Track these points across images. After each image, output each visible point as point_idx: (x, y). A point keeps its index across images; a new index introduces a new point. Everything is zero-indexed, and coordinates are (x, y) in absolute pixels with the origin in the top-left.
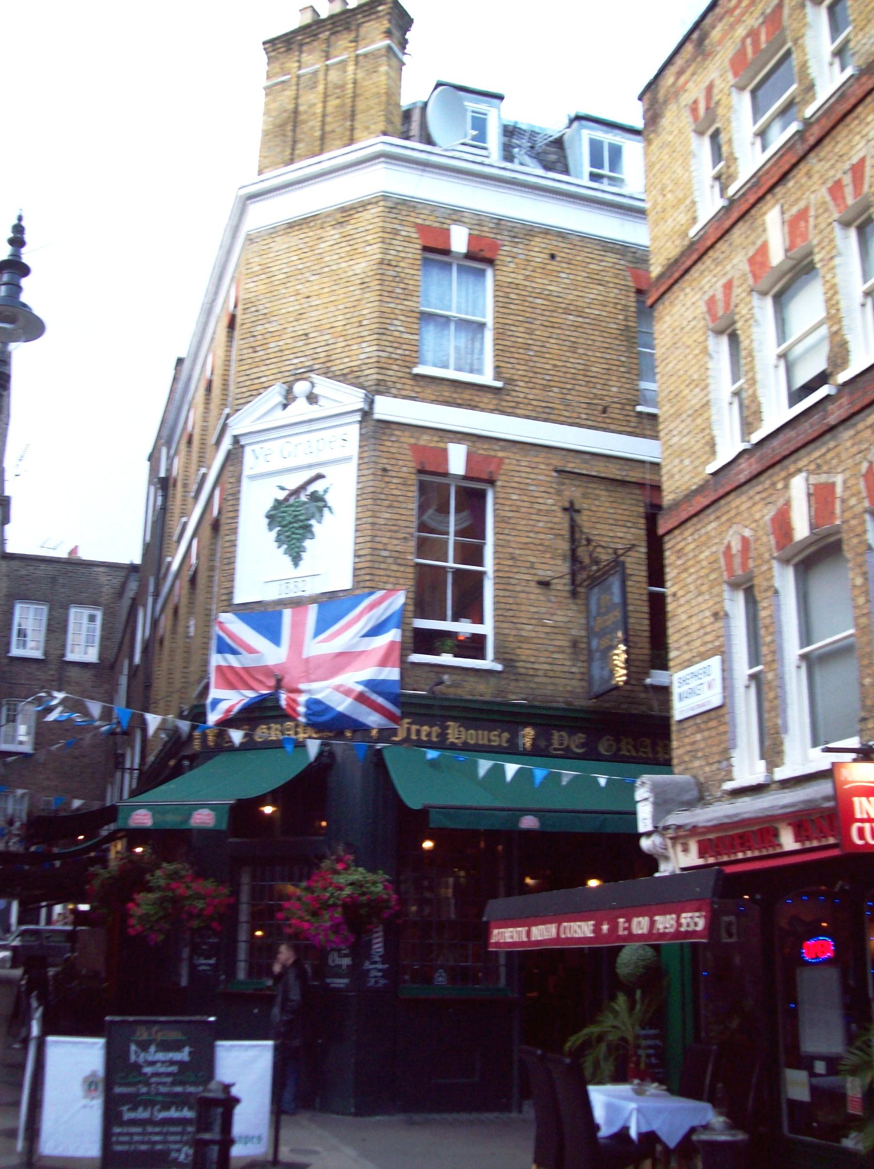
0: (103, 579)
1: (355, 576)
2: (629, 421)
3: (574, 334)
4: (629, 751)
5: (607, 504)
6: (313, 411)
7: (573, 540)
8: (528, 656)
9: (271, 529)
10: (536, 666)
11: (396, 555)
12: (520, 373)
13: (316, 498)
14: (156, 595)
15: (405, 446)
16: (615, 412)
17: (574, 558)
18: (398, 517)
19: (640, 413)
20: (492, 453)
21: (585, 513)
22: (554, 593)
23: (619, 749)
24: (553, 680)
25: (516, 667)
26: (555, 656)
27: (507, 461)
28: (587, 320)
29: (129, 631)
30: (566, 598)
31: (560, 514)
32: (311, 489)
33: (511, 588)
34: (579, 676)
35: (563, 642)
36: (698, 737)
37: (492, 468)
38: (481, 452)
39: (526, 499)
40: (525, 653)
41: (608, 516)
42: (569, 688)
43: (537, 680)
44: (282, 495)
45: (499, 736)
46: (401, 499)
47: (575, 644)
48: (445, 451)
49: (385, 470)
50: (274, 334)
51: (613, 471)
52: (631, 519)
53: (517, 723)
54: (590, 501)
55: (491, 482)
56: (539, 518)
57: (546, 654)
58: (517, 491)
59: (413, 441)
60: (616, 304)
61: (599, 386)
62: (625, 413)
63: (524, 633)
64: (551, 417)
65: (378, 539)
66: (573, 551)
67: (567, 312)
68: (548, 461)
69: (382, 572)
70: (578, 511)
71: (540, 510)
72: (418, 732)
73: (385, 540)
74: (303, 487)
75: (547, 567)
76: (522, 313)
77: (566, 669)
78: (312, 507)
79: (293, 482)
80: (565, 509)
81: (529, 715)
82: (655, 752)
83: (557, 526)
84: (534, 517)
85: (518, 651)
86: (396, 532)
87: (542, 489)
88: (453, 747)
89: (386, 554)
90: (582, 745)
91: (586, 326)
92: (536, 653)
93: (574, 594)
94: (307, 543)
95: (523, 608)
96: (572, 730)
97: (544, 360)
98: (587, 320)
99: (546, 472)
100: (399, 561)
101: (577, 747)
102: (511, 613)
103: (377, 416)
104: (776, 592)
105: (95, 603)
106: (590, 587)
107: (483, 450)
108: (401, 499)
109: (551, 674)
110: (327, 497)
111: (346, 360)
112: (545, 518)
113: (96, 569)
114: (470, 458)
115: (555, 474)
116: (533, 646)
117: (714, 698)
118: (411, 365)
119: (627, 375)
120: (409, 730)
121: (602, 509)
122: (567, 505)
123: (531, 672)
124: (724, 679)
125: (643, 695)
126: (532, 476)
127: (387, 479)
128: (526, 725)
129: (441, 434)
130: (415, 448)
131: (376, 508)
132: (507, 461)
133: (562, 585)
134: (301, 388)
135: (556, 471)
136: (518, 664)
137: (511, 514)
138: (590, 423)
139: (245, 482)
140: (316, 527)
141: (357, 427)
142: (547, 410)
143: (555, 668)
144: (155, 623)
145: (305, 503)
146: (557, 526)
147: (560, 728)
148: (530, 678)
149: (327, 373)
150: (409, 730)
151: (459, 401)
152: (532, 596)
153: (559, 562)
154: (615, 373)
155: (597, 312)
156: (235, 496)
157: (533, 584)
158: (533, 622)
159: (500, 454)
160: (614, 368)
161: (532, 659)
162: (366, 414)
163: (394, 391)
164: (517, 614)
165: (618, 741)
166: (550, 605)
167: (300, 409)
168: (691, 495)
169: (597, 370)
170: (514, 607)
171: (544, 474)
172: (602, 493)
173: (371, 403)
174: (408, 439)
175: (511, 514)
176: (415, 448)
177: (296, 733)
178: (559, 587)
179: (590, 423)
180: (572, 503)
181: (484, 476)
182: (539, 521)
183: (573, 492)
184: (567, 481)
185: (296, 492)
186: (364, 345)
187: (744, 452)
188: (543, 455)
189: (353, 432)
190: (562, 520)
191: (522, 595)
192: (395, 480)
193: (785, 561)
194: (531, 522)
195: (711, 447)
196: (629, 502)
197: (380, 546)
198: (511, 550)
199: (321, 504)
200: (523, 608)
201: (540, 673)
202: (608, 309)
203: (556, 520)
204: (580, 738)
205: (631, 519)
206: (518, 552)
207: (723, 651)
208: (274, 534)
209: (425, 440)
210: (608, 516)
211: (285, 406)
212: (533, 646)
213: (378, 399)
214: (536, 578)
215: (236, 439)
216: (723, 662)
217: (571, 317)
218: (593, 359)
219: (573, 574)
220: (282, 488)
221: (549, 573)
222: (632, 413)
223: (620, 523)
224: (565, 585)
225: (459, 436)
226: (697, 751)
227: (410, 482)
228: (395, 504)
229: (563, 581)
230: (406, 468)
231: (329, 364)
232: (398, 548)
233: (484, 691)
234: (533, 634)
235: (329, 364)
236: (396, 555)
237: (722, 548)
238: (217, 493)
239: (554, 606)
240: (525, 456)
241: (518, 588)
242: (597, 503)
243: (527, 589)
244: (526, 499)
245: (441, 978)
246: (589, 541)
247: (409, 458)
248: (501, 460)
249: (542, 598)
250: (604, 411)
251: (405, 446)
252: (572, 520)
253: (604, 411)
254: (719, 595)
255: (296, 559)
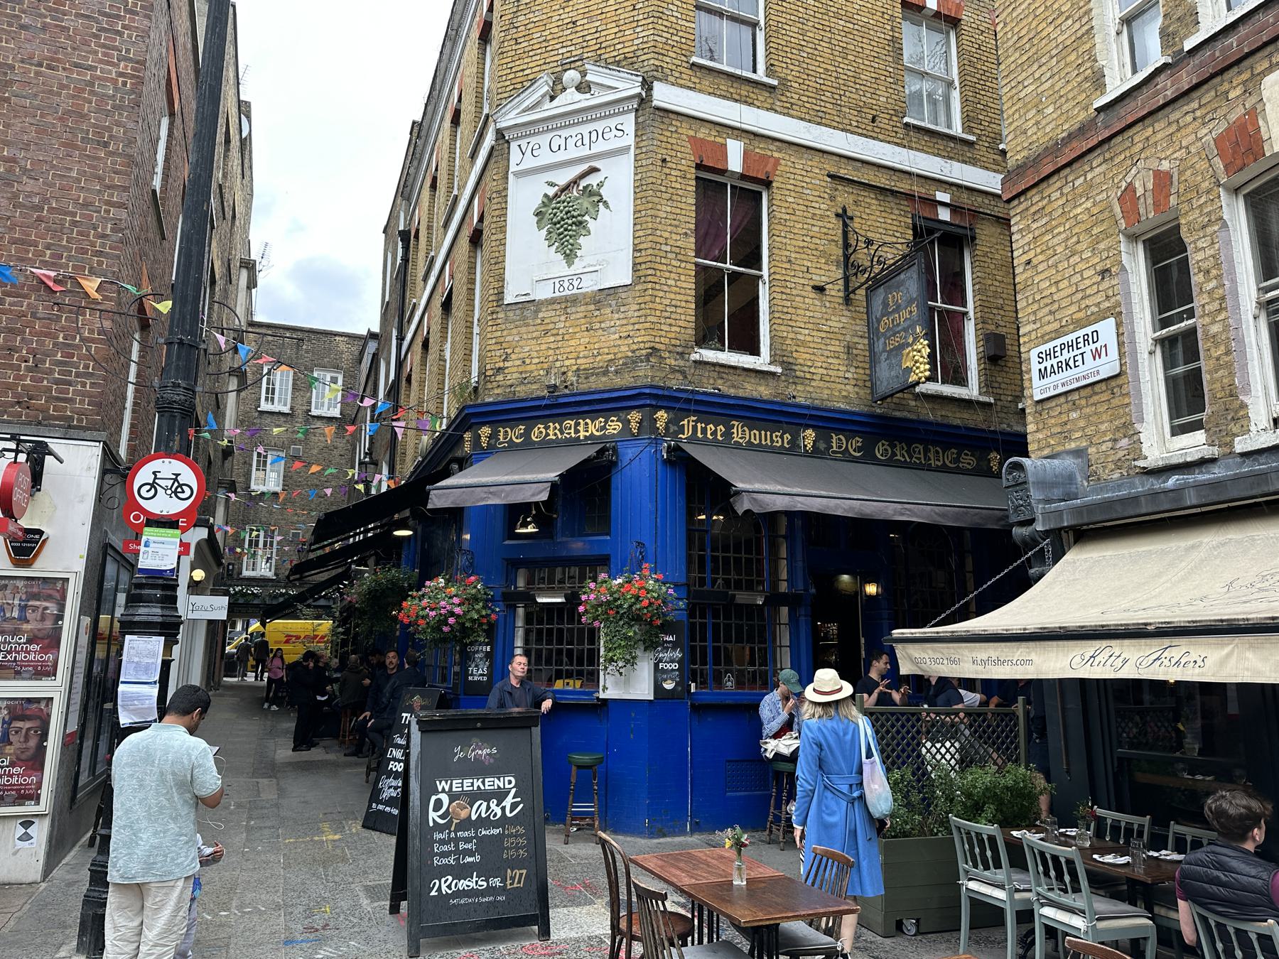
0: (343, 347)
1: (634, 271)
2: (896, 132)
3: (844, 39)
4: (904, 457)
5: (878, 213)
6: (584, 100)
7: (846, 245)
8: (805, 360)
9: (540, 228)
10: (812, 370)
11: (677, 250)
12: (793, 73)
13: (588, 192)
14: (401, 339)
15: (684, 137)
16: (883, 121)
17: (847, 261)
18: (678, 211)
19: (907, 125)
20: (769, 153)
21: (856, 220)
22: (828, 298)
23: (894, 454)
24: (827, 384)
25: (795, 370)
26: (830, 360)
27: (783, 162)
28: (856, 27)
29: (372, 378)
30: (839, 304)
31: (834, 220)
32: (583, 183)
33: (788, 291)
34: (853, 382)
35: (837, 347)
36: (1074, 415)
37: (769, 168)
38: (757, 150)
39: (801, 202)
40: (802, 357)
41: (879, 224)
42: (844, 393)
43: (813, 384)
44: (551, 191)
45: (782, 437)
46: (680, 192)
47: (849, 348)
48: (724, 147)
49: (664, 161)
50: (537, 24)
51: (882, 180)
52: (900, 229)
53: (801, 425)
54: (862, 209)
55: (768, 184)
56: (814, 222)
57: (823, 359)
58: (792, 194)
59: (692, 133)
60: (883, 13)
61: (869, 95)
62: (891, 123)
63: (802, 338)
64: (824, 121)
65: (658, 233)
66: (847, 257)
67: (837, 16)
68: (821, 165)
69: (664, 268)
70: (851, 218)
71: (814, 214)
72: (704, 431)
73: (666, 235)
74: (575, 182)
75: (822, 272)
76: (796, 13)
77: (841, 374)
78: (586, 202)
79: (563, 177)
80: (837, 215)
81: (812, 417)
82: (927, 458)
83: (830, 232)
84: (809, 221)
85: (795, 355)
86: (676, 226)
87: (817, 193)
88: (738, 446)
89: (668, 248)
90: (859, 449)
91: (855, 32)
92: (813, 357)
93: (847, 301)
94: (582, 240)
95: (799, 312)
96: (850, 434)
97: (817, 64)
98: (856, 27)
99: (821, 177)
100: (680, 257)
101: (854, 451)
102: (789, 317)
103: (655, 103)
104: (1225, 225)
105: (337, 368)
106: (871, 290)
107: (760, 148)
108: (680, 192)
109: (827, 378)
110: (602, 191)
111: (618, 47)
112: (820, 223)
113: (337, 338)
114: (746, 154)
115: (829, 180)
116: (811, 351)
117: (1108, 366)
118: (688, 54)
119: (893, 86)
120: (695, 428)
121: (872, 217)
122: (840, 211)
123: (808, 376)
124: (1120, 344)
125: (913, 403)
126: (808, 180)
127: (667, 171)
128: (807, 427)
129: (718, 128)
130: (693, 140)
131: (656, 200)
132: (783, 162)
133: (835, 291)
134: (571, 76)
135: (829, 176)
136: (796, 368)
137: (788, 217)
138: (860, 131)
139: (511, 176)
140: (592, 224)
141: (631, 117)
142: (820, 114)
143: (830, 372)
144: (400, 364)
145: (577, 199)
146: (830, 232)
147: (838, 431)
148: (807, 382)
149: (598, 61)
150: (695, 428)
151: (735, 96)
152: (807, 300)
153: (834, 268)
154: (883, 83)
155: (866, 20)
156: (503, 194)
157: (810, 288)
158: (810, 326)
159: (776, 155)
160: (883, 78)
161: (809, 363)
162: (643, 101)
163: (672, 79)
164: (794, 317)
165: (893, 446)
166: (824, 310)
167: (570, 99)
168: (1036, 161)
169: (866, 78)
170: (790, 310)
171: (818, 179)
172: (870, 199)
173: (650, 89)
174: (686, 130)
175: (788, 217)
176: (693, 140)
177: (577, 431)
178: (833, 293)
179: (860, 131)
180: (844, 210)
181: (762, 176)
182: (813, 225)
183: (845, 197)
184: (840, 188)
185: (566, 188)
186: (639, 29)
187: (1165, 66)
188: (817, 159)
189: (629, 122)
190: (836, 226)
191: (798, 299)
192: (673, 172)
193: (1133, 238)
194: (805, 226)
195: (1098, 81)
196: (897, 212)
197: (661, 240)
198: (788, 254)
199: (596, 199)
200: (799, 312)
201: (818, 377)
202: (875, 17)
203: (831, 226)
204: (857, 441)
205: (900, 229)
206: (793, 255)
207: (1119, 315)
208: (544, 232)
209: (703, 133)
210: (879, 224)
211: (552, 98)
212: (811, 351)
213: (657, 86)
214: (812, 283)
215: (500, 134)
216: (1119, 325)
217: (841, 22)
218: (862, 67)
219: (846, 279)
220: (552, 184)
221: (824, 278)
222: (898, 125)
223: (891, 233)
224: (839, 291)
225: (736, 132)
226: (1070, 431)
227: (688, 176)
228: (675, 197)
229: (837, 287)
230: (685, 163)
231: (599, 52)
232: (679, 244)
233: (764, 391)
234: (809, 339)
235: (599, 52)
236: (677, 250)
237: (1115, 194)
238: (476, 201)
239: (829, 311)
240: (801, 158)
241: (794, 292)
242: (867, 211)
243: (803, 293)
244: (801, 202)
245: (729, 683)
246: (869, 242)
247: (688, 151)
248: (777, 160)
249: (817, 302)
250: (873, 121)
251: (684, 137)
252: (845, 225)
253: (873, 121)
254: (1115, 247)
255: (570, 257)
